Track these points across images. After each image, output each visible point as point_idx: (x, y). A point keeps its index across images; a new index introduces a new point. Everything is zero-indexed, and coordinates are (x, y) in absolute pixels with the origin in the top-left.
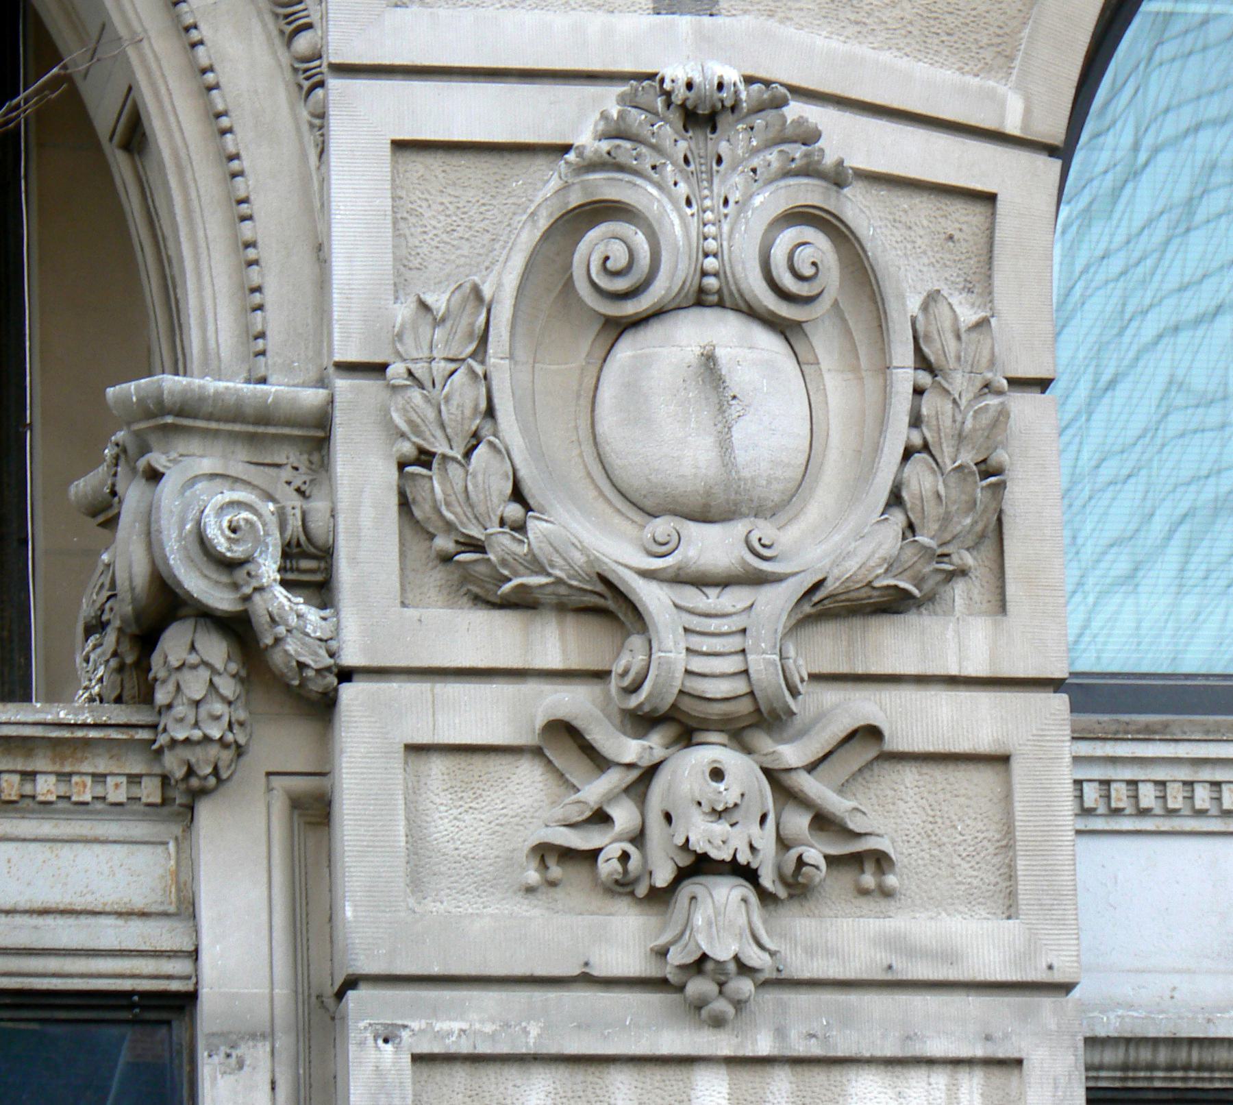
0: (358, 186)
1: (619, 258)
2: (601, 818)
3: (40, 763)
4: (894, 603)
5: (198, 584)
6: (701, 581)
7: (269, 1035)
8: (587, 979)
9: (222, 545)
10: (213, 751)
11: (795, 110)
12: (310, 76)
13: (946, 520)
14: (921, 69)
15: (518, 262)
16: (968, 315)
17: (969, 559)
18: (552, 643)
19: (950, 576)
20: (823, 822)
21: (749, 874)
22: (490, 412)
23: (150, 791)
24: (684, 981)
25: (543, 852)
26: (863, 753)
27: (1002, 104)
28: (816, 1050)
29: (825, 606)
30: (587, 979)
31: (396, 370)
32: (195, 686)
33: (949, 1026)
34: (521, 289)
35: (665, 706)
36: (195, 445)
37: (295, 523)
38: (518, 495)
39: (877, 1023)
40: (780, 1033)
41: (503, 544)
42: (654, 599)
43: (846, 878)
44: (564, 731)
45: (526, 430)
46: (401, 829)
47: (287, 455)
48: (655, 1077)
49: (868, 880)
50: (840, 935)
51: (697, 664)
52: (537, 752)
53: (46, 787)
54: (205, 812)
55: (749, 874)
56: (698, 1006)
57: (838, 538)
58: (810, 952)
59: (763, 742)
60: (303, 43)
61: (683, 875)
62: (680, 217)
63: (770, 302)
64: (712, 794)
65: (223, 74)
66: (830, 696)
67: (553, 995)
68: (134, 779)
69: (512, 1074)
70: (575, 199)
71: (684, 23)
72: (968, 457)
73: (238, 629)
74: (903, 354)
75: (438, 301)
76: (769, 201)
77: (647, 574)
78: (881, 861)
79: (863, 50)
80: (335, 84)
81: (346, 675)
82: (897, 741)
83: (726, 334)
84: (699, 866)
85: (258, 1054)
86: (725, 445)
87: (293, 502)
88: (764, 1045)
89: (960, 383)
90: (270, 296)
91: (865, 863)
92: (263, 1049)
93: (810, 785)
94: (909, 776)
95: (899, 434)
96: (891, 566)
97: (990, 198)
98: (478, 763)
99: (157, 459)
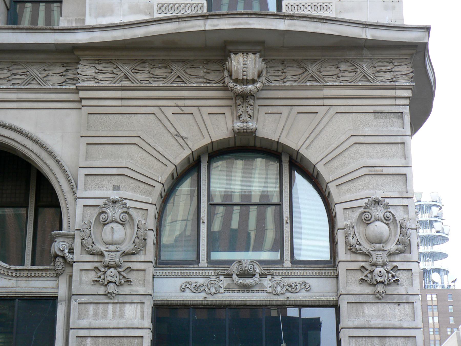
0: (79, 210)
1: (104, 217)
2: (100, 277)
3: (36, 272)
4: (133, 254)
5: (59, 253)
6: (111, 252)
7: (65, 301)
8: (98, 294)
9: (61, 249)
10: (60, 271)
11: (125, 201)
12: (76, 198)
13: (139, 244)
14: (141, 196)
15: (95, 218)
16: (143, 222)
17: (142, 249)
18: (96, 259)
19: (140, 251)
20: (124, 277)
21: (115, 283)
22: (91, 234)
23: (55, 275)
24: (108, 294)
25: (94, 281)
26: (129, 270)
27: (149, 200)
28: (122, 302)
29: (125, 254)
30: (98, 294)
31: (82, 230)
32: (59, 264)
33: (136, 299)
34: (95, 221)
35: (107, 264)
36: (61, 238)
37: (70, 246)
38: (93, 243)
39: (129, 299)
40: (118, 300)
41: (91, 248)
42: (106, 254)
43: (126, 284)
44: (96, 268)
45: (94, 236)
46: (79, 279)
47: (71, 239)
48: (104, 305)
49: (129, 283)
50: (126, 289)
51: (110, 261)
52: (94, 270)
53: (44, 275)
54: (60, 277)
55: (115, 283)
56: (109, 297)
57: (127, 247)
58: (122, 291)
59: (386, 267)
60: (75, 195)
61: (108, 283)
62: (111, 213)
63: (120, 222)
64: (112, 274)
65: (67, 199)
66: (126, 264)
67: (94, 296)
68: (53, 274)
69: (89, 305)
70: (100, 211)
71: (115, 192)
72: (142, 238)
73: (63, 257)
74: (136, 227)
75: (86, 222)
76: (120, 211)
77: (105, 251)
78: (130, 281)
79: (135, 195)
80: (78, 200)
81: (74, 262)
82: (132, 268)
83: (114, 225)
84: (109, 282)
85: (64, 303)
86: (113, 237)
87: (71, 244)
88: (116, 302)
89: (142, 230)
90: (70, 222)
91: (128, 282)
92: (64, 302)
93: (123, 273)
94: (135, 272)
95: (135, 235)
96: (132, 250)
97: (147, 210)
98: (88, 271)
99: (56, 240)
